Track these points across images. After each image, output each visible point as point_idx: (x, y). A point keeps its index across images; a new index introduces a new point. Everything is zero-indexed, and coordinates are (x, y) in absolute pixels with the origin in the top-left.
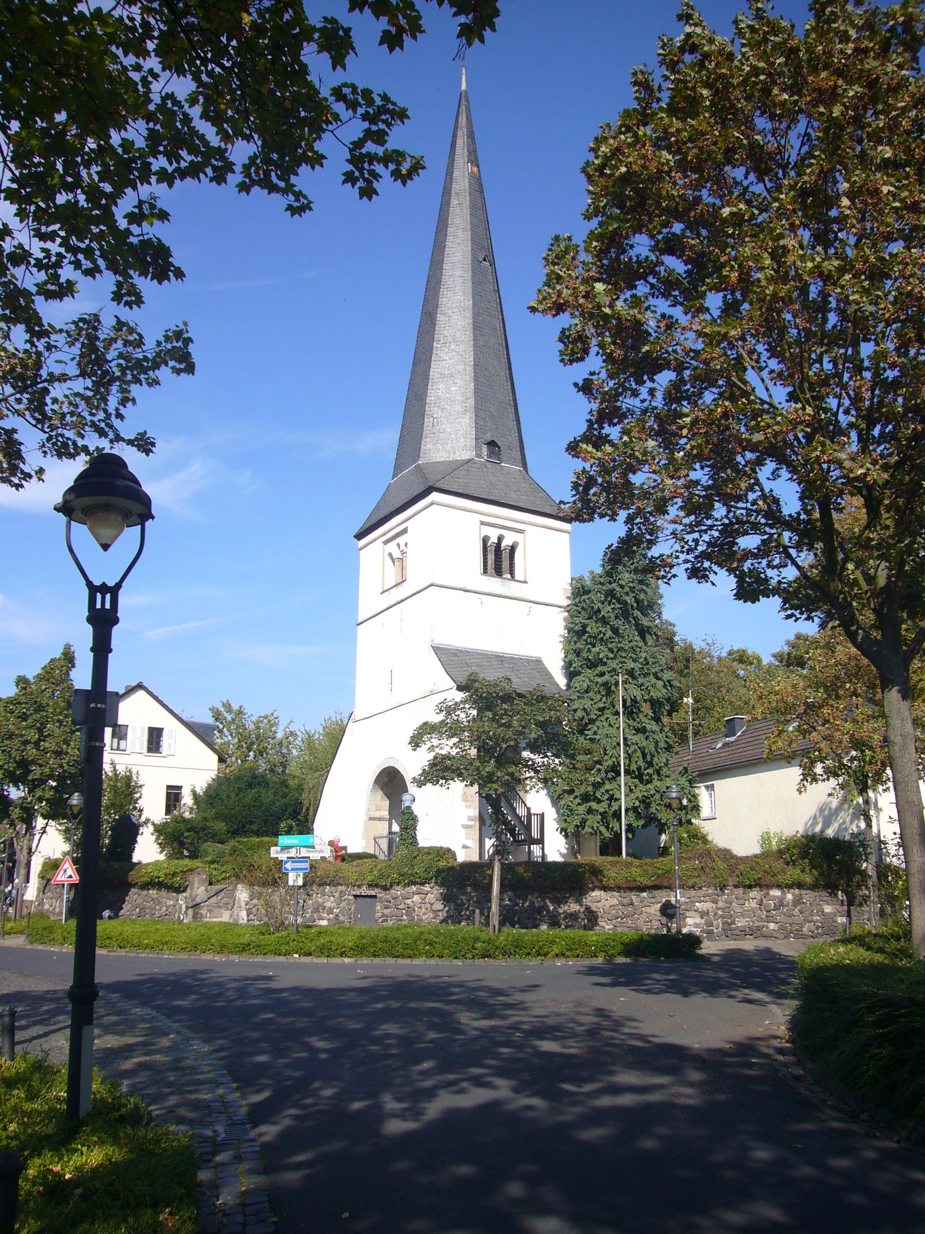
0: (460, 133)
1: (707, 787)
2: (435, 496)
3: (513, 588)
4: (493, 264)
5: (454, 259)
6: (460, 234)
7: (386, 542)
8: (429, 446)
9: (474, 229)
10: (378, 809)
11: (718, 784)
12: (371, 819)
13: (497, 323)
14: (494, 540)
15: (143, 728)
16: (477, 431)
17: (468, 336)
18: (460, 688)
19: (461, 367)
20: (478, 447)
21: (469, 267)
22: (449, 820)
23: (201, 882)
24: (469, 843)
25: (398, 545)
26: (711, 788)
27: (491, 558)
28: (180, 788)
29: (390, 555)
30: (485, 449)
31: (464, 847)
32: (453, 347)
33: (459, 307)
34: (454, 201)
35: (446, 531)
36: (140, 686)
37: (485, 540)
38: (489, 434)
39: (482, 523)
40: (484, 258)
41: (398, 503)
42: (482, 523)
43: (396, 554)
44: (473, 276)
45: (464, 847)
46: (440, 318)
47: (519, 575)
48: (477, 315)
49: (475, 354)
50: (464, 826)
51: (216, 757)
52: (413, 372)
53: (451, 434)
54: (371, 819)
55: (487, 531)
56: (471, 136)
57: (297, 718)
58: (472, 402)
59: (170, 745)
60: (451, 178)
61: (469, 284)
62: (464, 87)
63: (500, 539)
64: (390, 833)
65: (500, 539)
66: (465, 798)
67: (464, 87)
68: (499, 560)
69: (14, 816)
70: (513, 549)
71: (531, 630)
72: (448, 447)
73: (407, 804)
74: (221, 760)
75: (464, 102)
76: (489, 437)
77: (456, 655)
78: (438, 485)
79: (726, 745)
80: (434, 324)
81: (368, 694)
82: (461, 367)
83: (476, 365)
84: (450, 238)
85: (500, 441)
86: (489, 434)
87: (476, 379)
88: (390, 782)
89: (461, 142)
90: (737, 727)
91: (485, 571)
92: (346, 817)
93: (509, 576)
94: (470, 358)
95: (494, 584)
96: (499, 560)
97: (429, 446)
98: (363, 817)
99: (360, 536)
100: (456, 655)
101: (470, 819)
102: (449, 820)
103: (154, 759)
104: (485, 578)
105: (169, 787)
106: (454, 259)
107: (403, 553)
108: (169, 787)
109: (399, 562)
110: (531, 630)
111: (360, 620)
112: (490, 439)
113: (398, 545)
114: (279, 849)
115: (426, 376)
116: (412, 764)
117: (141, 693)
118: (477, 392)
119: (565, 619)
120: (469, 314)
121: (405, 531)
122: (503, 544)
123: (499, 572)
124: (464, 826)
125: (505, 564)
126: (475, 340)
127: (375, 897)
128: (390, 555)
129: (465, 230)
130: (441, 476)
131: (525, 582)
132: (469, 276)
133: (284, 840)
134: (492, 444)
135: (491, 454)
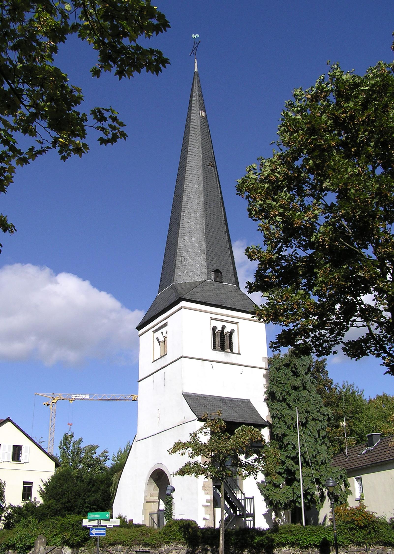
0: (194, 94)
1: (357, 479)
2: (183, 303)
3: (232, 358)
4: (215, 166)
5: (192, 165)
6: (195, 150)
7: (155, 332)
8: (180, 274)
9: (203, 147)
10: (152, 495)
11: (364, 477)
12: (147, 502)
13: (219, 200)
14: (219, 328)
15: (9, 446)
16: (208, 264)
17: (202, 208)
18: (200, 420)
19: (198, 227)
20: (208, 274)
21: (201, 169)
22: (195, 502)
23: (41, 543)
24: (208, 517)
25: (162, 333)
26: (359, 480)
27: (218, 339)
28: (31, 483)
29: (157, 339)
30: (213, 274)
31: (204, 519)
32: (192, 215)
33: (196, 192)
34: (192, 132)
35: (190, 324)
36: (8, 420)
37: (214, 329)
38: (215, 266)
39: (212, 319)
40: (211, 164)
41: (162, 308)
42: (212, 319)
43: (161, 339)
44: (204, 173)
45: (204, 519)
46: (185, 198)
47: (235, 350)
48: (206, 195)
49: (206, 218)
50: (204, 506)
51: (54, 464)
52: (170, 230)
53: (193, 267)
54: (147, 502)
55: (215, 323)
56: (201, 95)
57: (108, 448)
58: (204, 247)
59: (26, 456)
60: (190, 119)
61: (201, 179)
62: (196, 69)
63: (223, 328)
64: (159, 511)
65: (223, 328)
66: (204, 488)
67: (196, 69)
68: (223, 341)
69: (64, 533)
70: (231, 333)
71: (244, 377)
72: (191, 274)
73: (168, 492)
74: (57, 466)
75: (196, 77)
76: (215, 267)
77: (197, 399)
78: (185, 297)
79: (368, 452)
80: (181, 202)
81: (145, 423)
82: (198, 227)
83: (206, 225)
84: (189, 153)
85: (222, 271)
86: (215, 266)
87: (207, 233)
88: (159, 478)
89: (195, 99)
90: (374, 440)
91: (215, 348)
92: (132, 502)
93: (229, 350)
94: (203, 221)
95: (220, 355)
96: (223, 341)
97: (180, 274)
98: (143, 501)
99: (139, 328)
100: (197, 399)
101: (208, 501)
102: (195, 502)
103: (16, 465)
104: (215, 352)
105: (25, 483)
106: (192, 165)
107: (165, 337)
108: (25, 483)
109: (163, 343)
110: (244, 377)
111: (140, 379)
112: (215, 268)
113: (162, 333)
114: (87, 520)
115: (177, 233)
116: (172, 464)
117: (9, 423)
118: (208, 241)
119: (264, 376)
120: (202, 195)
121: (166, 325)
122: (225, 331)
123: (223, 349)
124: (204, 506)
125: (227, 343)
126: (206, 210)
127: (149, 552)
128: (157, 339)
129: (198, 147)
130: (186, 291)
131: (239, 354)
132: (201, 173)
133: (91, 515)
134: (217, 271)
135: (216, 276)
